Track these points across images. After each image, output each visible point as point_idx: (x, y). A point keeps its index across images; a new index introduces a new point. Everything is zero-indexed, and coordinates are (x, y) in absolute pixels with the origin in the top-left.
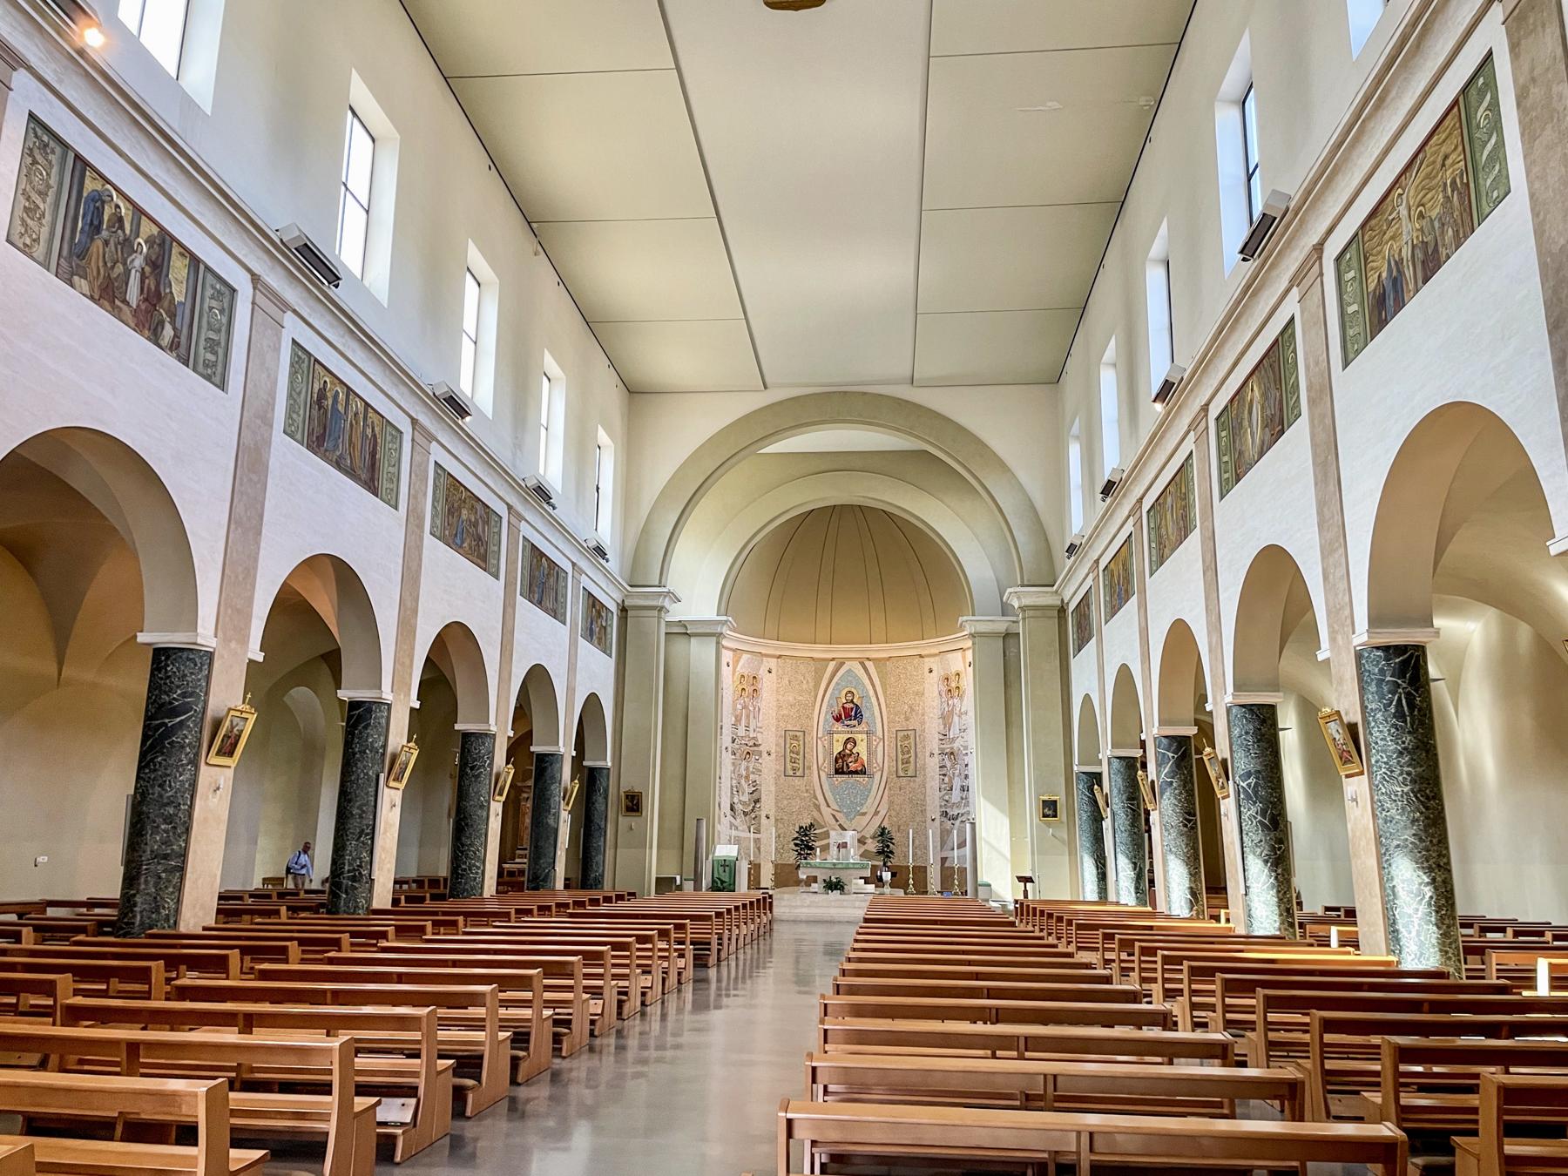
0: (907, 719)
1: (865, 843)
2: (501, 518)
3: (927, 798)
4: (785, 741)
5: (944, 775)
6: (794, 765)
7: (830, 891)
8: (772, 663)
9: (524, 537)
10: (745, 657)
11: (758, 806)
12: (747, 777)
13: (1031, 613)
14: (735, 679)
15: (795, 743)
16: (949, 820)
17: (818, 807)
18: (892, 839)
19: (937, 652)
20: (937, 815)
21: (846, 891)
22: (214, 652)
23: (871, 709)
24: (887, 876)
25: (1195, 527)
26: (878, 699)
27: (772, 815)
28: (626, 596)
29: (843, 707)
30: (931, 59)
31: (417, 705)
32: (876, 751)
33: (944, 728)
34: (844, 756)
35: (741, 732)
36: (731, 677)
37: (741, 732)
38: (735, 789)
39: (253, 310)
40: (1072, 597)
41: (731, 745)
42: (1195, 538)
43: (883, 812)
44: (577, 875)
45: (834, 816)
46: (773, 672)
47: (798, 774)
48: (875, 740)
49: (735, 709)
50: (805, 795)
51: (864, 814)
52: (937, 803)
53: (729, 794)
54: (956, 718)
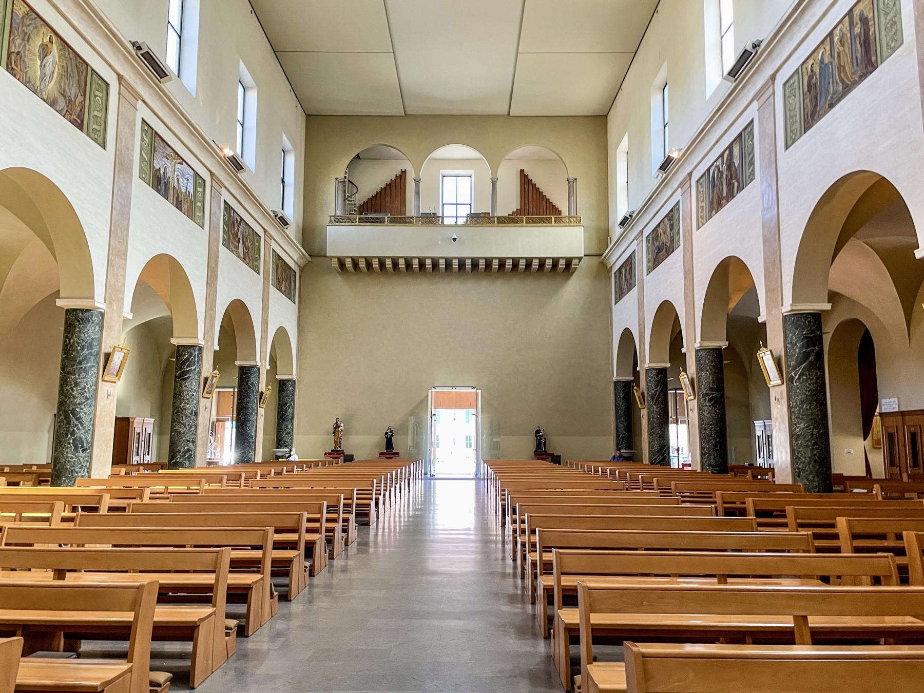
2: (260, 237)
9: (273, 249)
22: (104, 312)
25: (635, 285)
30: (519, 54)
31: (217, 348)
39: (211, 188)
42: (635, 290)
44: (891, 463)
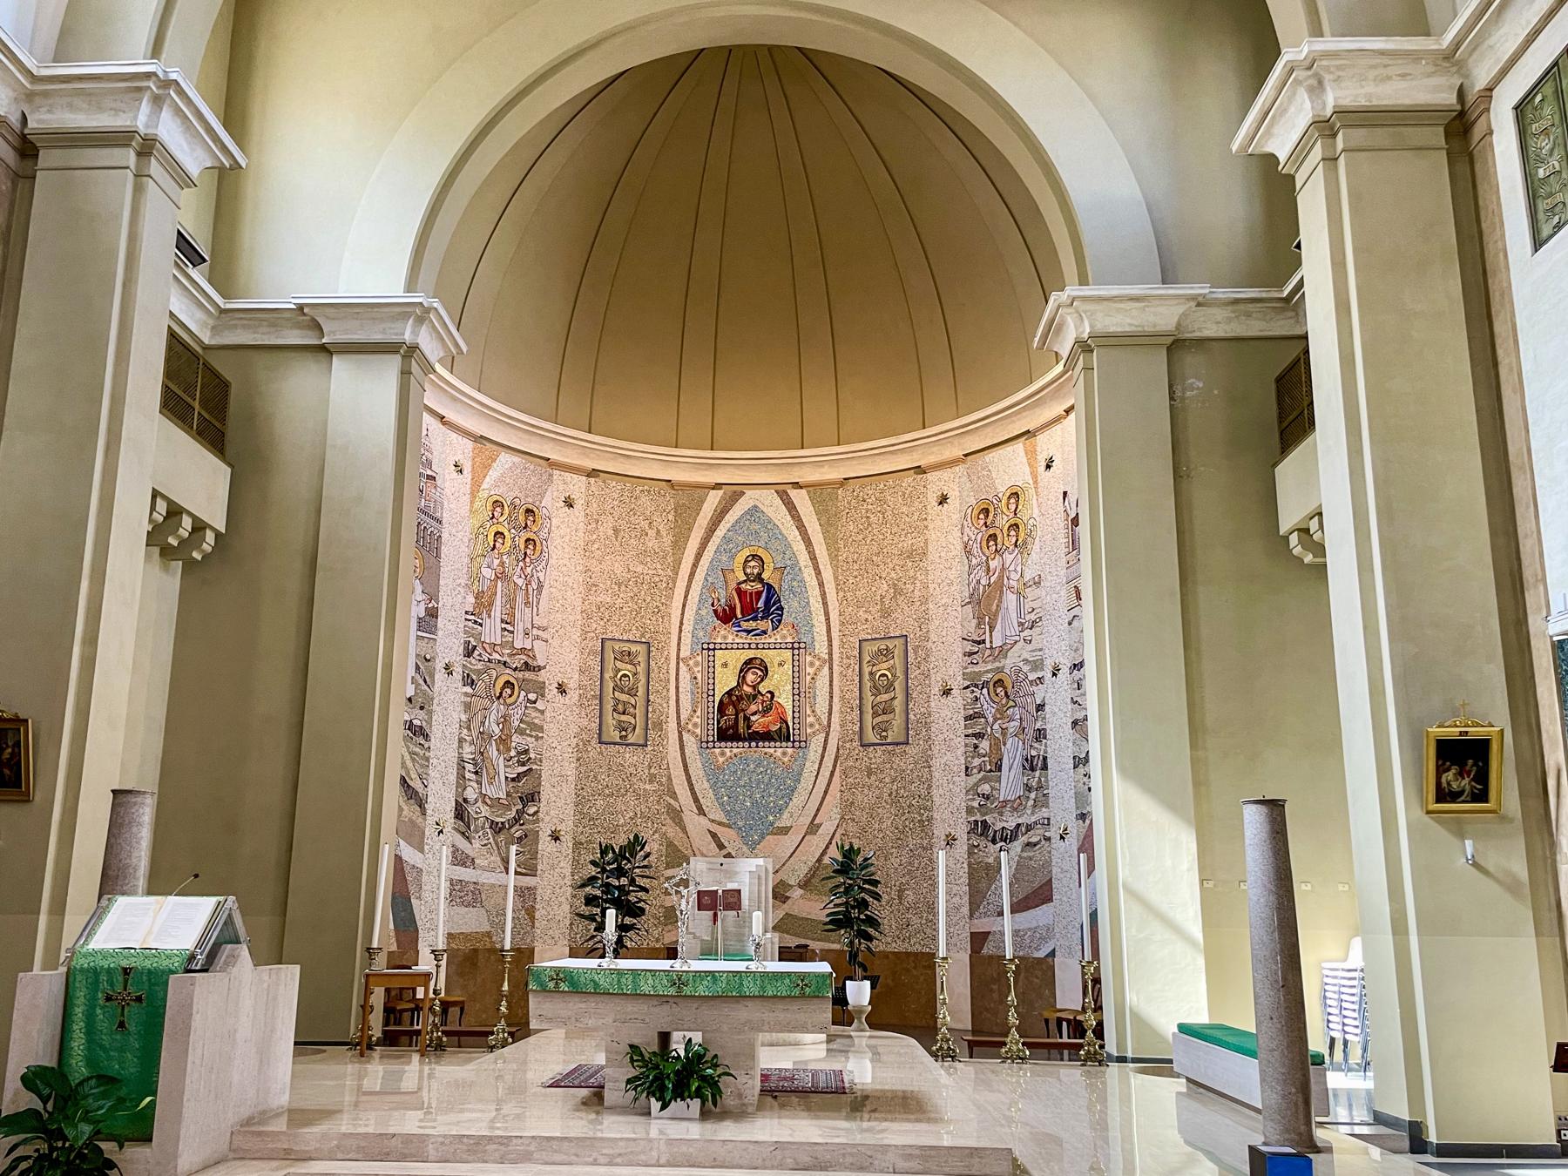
0: (886, 614)
1: (788, 898)
3: (934, 792)
4: (602, 661)
5: (979, 736)
6: (624, 718)
7: (655, 1105)
8: (577, 486)
10: (505, 459)
11: (532, 810)
12: (504, 741)
13: (1360, 136)
14: (477, 504)
15: (626, 669)
16: (994, 841)
17: (676, 816)
18: (875, 883)
19: (960, 453)
20: (961, 832)
21: (728, 1100)
23: (800, 592)
24: (859, 993)
26: (818, 573)
27: (566, 828)
28: (30, 96)
29: (739, 592)
32: (813, 687)
33: (979, 624)
34: (740, 698)
35: (492, 631)
36: (467, 498)
37: (492, 631)
38: (469, 767)
40: (1504, 72)
41: (465, 661)
43: (827, 828)
45: (714, 835)
46: (579, 504)
47: (631, 739)
48: (812, 664)
49: (475, 577)
50: (648, 787)
51: (785, 831)
52: (960, 801)
53: (453, 778)
54: (1010, 599)
